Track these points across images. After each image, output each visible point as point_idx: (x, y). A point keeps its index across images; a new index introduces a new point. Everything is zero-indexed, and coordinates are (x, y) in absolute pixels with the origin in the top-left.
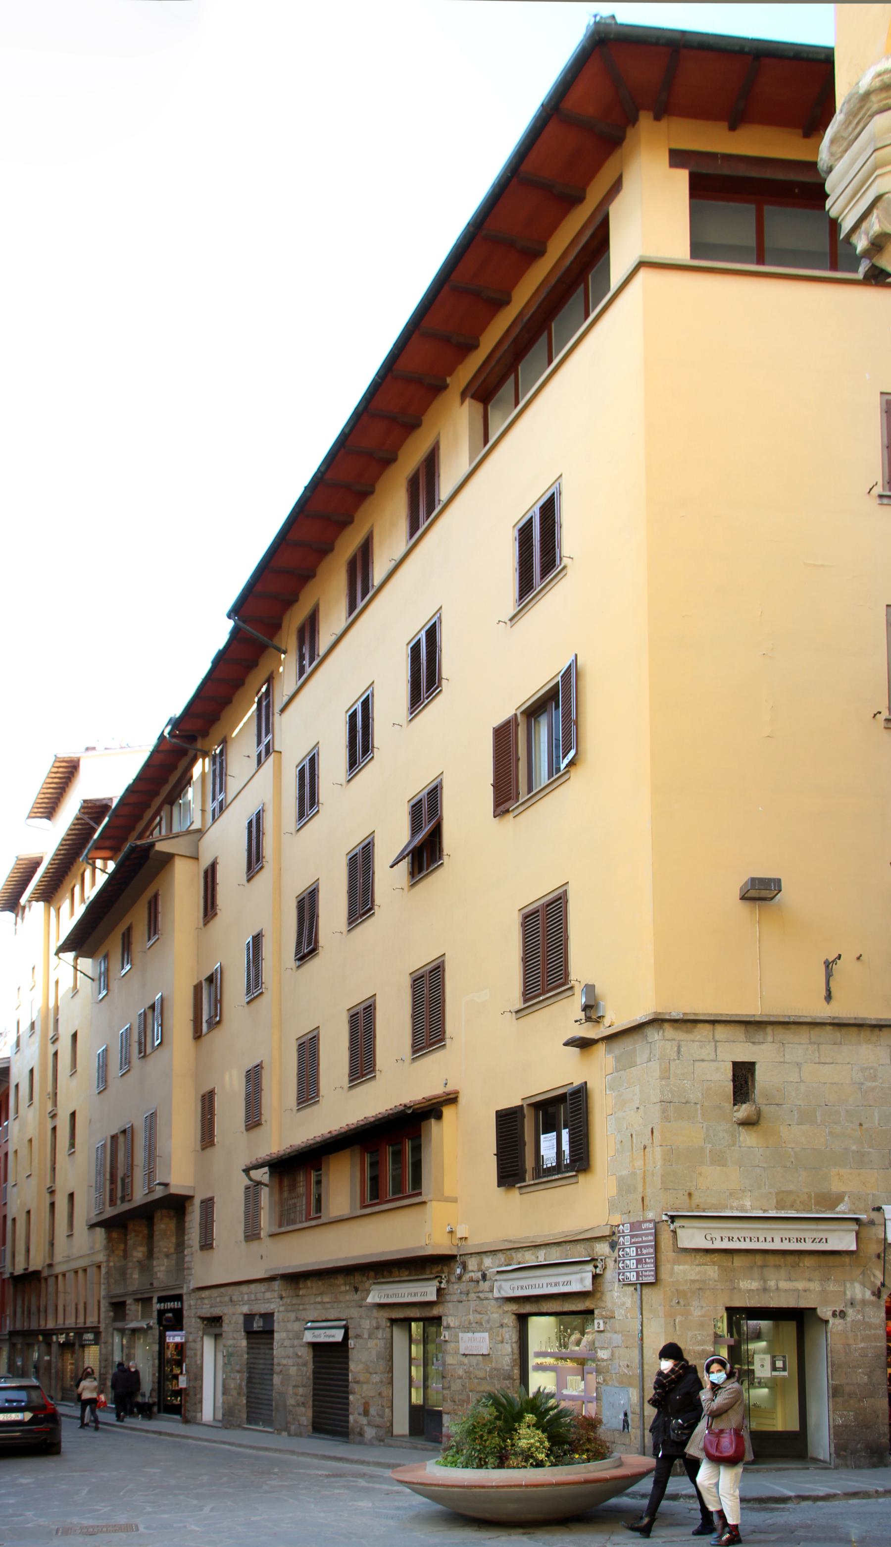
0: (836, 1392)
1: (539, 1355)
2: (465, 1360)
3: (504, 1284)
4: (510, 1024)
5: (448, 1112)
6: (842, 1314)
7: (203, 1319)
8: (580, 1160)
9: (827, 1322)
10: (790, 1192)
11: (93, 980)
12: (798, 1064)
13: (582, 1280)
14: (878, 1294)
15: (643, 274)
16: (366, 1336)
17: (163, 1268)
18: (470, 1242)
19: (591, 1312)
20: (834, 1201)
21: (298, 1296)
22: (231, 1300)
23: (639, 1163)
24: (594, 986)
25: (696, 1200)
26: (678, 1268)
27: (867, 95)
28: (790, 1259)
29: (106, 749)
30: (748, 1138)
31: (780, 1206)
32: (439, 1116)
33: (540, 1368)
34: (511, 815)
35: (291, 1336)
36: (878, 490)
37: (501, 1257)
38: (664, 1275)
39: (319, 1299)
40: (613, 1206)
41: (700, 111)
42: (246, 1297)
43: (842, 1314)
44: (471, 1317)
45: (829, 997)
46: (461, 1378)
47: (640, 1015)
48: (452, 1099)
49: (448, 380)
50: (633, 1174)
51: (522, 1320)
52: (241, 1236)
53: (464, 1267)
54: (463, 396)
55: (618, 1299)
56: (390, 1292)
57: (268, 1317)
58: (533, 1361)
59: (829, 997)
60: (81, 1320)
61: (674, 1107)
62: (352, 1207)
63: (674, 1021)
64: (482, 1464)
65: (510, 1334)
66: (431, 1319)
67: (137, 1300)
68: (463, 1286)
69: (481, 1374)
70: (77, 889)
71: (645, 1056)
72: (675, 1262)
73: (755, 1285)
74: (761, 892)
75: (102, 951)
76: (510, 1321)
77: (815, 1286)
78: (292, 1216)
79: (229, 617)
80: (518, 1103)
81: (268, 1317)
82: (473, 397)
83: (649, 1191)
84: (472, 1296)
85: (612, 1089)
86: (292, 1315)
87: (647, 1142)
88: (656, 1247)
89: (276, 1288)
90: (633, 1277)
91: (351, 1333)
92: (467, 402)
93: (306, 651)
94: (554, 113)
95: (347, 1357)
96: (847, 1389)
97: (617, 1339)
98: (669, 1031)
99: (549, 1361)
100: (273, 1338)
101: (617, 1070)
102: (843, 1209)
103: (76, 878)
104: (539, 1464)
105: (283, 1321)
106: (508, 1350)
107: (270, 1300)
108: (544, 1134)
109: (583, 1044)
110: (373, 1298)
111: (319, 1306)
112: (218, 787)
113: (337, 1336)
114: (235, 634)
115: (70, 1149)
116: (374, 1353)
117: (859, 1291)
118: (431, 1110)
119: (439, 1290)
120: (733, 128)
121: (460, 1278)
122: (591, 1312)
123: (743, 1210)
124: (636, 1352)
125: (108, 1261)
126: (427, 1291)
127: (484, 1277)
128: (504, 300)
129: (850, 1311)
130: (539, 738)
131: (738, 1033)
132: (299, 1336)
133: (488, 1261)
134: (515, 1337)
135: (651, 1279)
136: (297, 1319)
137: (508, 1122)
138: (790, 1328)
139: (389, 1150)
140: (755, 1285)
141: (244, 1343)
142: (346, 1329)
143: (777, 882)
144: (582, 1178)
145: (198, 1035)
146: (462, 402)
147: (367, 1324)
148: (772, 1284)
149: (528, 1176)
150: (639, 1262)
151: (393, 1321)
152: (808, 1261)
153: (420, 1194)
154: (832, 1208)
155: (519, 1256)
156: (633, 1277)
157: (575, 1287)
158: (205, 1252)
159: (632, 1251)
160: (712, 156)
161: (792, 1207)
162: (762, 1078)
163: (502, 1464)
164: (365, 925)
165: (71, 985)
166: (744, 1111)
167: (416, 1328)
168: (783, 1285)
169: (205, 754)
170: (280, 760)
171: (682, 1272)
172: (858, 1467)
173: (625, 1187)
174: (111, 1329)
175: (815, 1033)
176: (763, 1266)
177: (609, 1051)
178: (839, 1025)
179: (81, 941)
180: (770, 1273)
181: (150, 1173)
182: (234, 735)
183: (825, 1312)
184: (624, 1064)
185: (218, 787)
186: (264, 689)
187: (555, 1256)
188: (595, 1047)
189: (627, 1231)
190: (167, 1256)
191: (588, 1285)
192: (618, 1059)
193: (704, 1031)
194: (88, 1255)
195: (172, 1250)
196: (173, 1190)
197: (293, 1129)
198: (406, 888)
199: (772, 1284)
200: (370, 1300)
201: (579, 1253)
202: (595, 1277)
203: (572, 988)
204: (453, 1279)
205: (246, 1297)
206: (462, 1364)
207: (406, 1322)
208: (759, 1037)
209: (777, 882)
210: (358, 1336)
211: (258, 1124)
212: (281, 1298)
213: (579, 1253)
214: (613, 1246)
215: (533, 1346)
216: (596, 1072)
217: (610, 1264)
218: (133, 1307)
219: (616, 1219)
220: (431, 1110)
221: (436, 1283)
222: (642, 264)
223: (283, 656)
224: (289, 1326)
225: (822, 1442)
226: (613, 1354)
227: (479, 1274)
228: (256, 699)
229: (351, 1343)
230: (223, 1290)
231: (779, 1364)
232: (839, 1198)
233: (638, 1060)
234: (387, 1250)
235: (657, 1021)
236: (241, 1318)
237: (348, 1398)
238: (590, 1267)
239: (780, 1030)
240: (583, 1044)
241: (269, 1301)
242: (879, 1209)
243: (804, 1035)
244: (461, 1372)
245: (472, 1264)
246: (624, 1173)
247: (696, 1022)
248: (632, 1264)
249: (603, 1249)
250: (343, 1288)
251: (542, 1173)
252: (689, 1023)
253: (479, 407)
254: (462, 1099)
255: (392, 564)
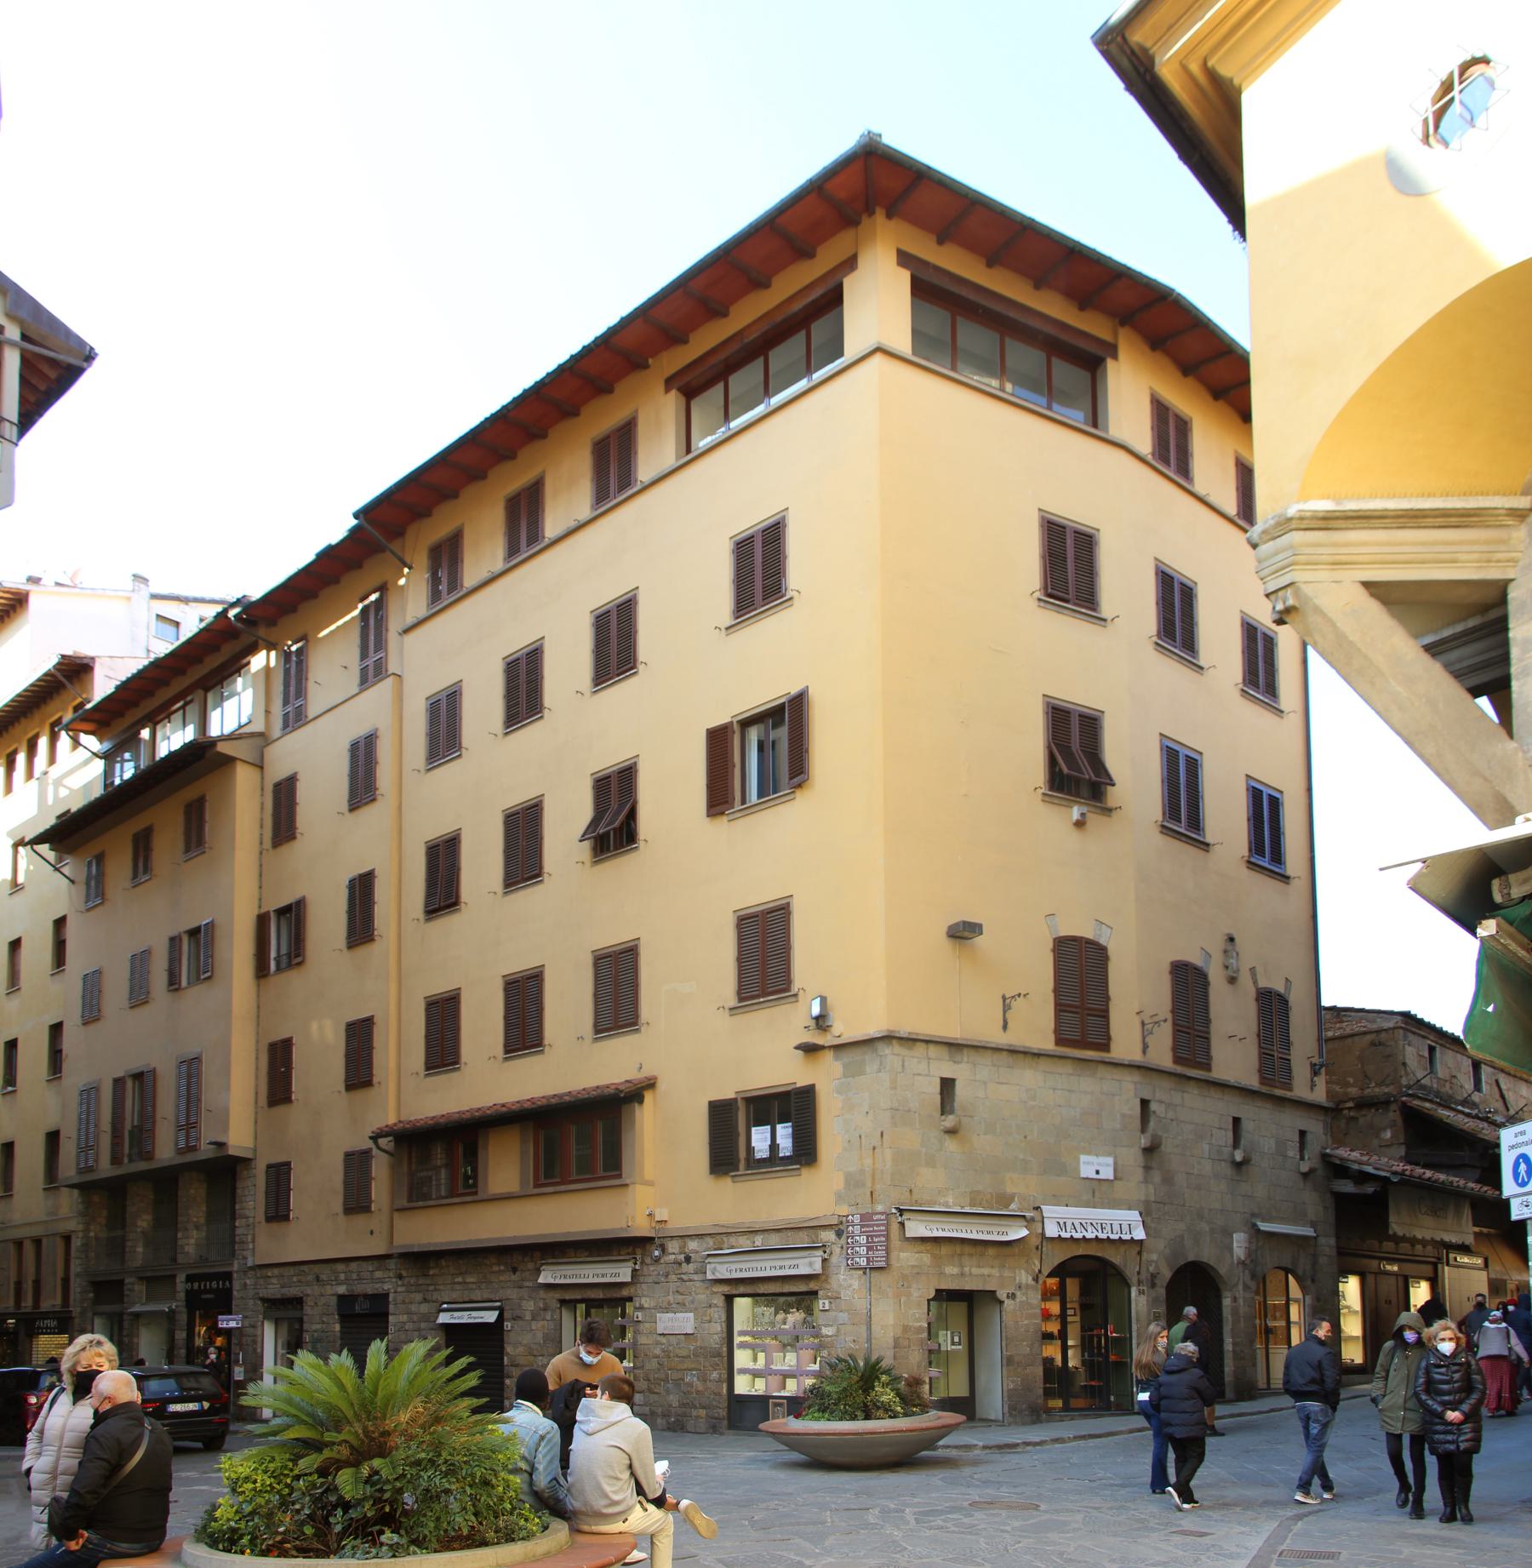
0: (1008, 1361)
1: (742, 1333)
2: (663, 1340)
3: (719, 1267)
4: (724, 1021)
5: (648, 1097)
6: (1012, 1296)
7: (263, 1300)
8: (806, 1151)
9: (1001, 1302)
10: (979, 1192)
11: (72, 882)
12: (985, 1083)
13: (811, 1264)
14: (1036, 1279)
15: (878, 358)
16: (528, 1317)
17: (192, 1241)
18: (669, 1226)
19: (816, 1293)
20: (1006, 1200)
21: (425, 1275)
22: (318, 1279)
23: (868, 1162)
24: (953, 1081)
25: (915, 1197)
26: (903, 1255)
27: (1290, 519)
28: (979, 1249)
29: (58, 584)
30: (951, 1144)
31: (972, 1205)
32: (641, 1101)
33: (743, 1345)
34: (725, 819)
35: (415, 1318)
36: (1038, 594)
37: (710, 1241)
38: (893, 1262)
39: (460, 1279)
40: (840, 1198)
41: (919, 221)
42: (342, 1276)
43: (1012, 1296)
44: (671, 1298)
45: (1005, 1027)
46: (657, 1357)
47: (872, 1030)
48: (651, 1084)
49: (650, 361)
50: (862, 1172)
51: (729, 1299)
52: (337, 1204)
53: (663, 1249)
54: (669, 383)
55: (847, 1284)
56: (569, 1273)
57: (383, 1298)
58: (737, 1339)
59: (1005, 1027)
60: (28, 1303)
61: (900, 1114)
62: (523, 1183)
63: (900, 1039)
64: (854, 1418)
65: (719, 1314)
66: (614, 1299)
67: (141, 1279)
68: (661, 1269)
69: (684, 1353)
70: (21, 758)
71: (876, 1067)
72: (901, 1250)
73: (955, 1271)
74: (963, 932)
75: (95, 847)
76: (720, 1301)
77: (995, 1272)
78: (425, 1189)
79: (356, 516)
80: (733, 1096)
81: (383, 1298)
82: (679, 390)
83: (878, 1187)
84: (673, 1277)
85: (839, 1092)
86: (419, 1297)
87: (878, 1144)
88: (888, 1237)
89: (393, 1266)
90: (863, 1262)
91: (506, 1315)
92: (674, 392)
93: (443, 574)
94: (817, 190)
95: (502, 1341)
96: (1017, 1359)
97: (843, 1317)
98: (896, 1048)
99: (747, 1338)
100: (387, 1322)
101: (845, 1076)
102: (1014, 1208)
103: (19, 741)
104: (895, 1416)
105: (404, 1302)
106: (718, 1327)
107: (385, 1282)
108: (762, 1126)
109: (810, 1049)
110: (546, 1277)
111: (458, 1287)
112: (292, 689)
113: (490, 1317)
114: (354, 532)
115: (4, 1087)
116: (540, 1335)
117: (1025, 1278)
118: (632, 1095)
119: (634, 1271)
120: (940, 242)
121: (657, 1260)
122: (816, 1293)
123: (947, 1205)
124: (864, 1328)
125: (87, 1230)
126: (623, 1273)
127: (688, 1260)
128: (736, 323)
129: (1018, 1294)
130: (763, 753)
131: (943, 1052)
132: (430, 1318)
133: (692, 1245)
134: (724, 1318)
135: (883, 1264)
136: (425, 1300)
137: (723, 1117)
138: (960, 1309)
139: (573, 1129)
140: (955, 1271)
141: (338, 1327)
142: (501, 1310)
143: (980, 926)
144: (805, 1172)
145: (261, 970)
146: (667, 390)
147: (529, 1306)
148: (967, 1269)
149: (742, 1165)
150: (869, 1249)
151: (563, 1302)
152: (991, 1251)
153: (620, 1176)
154: (1007, 1206)
155: (733, 1240)
156: (863, 1262)
157: (804, 1270)
158: (275, 1226)
159: (863, 1239)
160: (937, 269)
161: (980, 1205)
162: (961, 1091)
163: (867, 1417)
164: (530, 890)
165: (9, 876)
166: (949, 1121)
167: (581, 1307)
168: (975, 1271)
169: (270, 646)
170: (401, 683)
171: (906, 1258)
172: (1024, 1424)
173: (852, 1182)
174: (90, 1314)
175: (997, 1056)
176: (961, 1255)
177: (836, 1058)
178: (1013, 1052)
179: (68, 834)
180: (966, 1260)
181: (189, 1125)
182: (322, 634)
183: (1002, 1295)
184: (852, 1072)
185: (292, 689)
186: (373, 597)
187: (774, 1241)
188: (822, 1053)
189: (857, 1221)
190: (197, 1228)
191: (817, 1268)
192: (845, 1066)
193: (921, 1047)
194: (46, 1222)
195: (202, 1220)
196: (231, 1152)
197: (412, 1094)
198: (588, 863)
199: (967, 1269)
200: (541, 1280)
201: (802, 1240)
202: (824, 1260)
203: (795, 995)
204: (648, 1260)
205: (342, 1276)
206: (658, 1343)
207: (569, 1304)
208: (958, 1058)
209: (980, 926)
210: (515, 1318)
211: (368, 1083)
212: (400, 1277)
213: (802, 1240)
214: (839, 1234)
215: (737, 1327)
216: (825, 1076)
217: (837, 1250)
218: (137, 1287)
219: (844, 1210)
220: (632, 1095)
221: (631, 1264)
222: (879, 350)
223: (406, 570)
224: (414, 1308)
225: (993, 1401)
226: (838, 1330)
227: (682, 1257)
228: (360, 606)
229: (508, 1325)
230: (305, 1268)
231: (956, 1339)
232: (1011, 1199)
233: (868, 1069)
234: (573, 1230)
235: (889, 1038)
236: (334, 1301)
237: (503, 1383)
238: (820, 1253)
239: (972, 1052)
240: (810, 1049)
241: (381, 1281)
242: (1037, 1208)
243: (986, 1059)
244: (657, 1351)
245: (673, 1246)
246: (853, 1169)
247: (915, 1040)
248: (863, 1251)
249: (828, 1236)
250: (496, 1268)
251: (758, 1166)
252: (910, 1041)
253: (683, 400)
254: (661, 1085)
255: (573, 524)
